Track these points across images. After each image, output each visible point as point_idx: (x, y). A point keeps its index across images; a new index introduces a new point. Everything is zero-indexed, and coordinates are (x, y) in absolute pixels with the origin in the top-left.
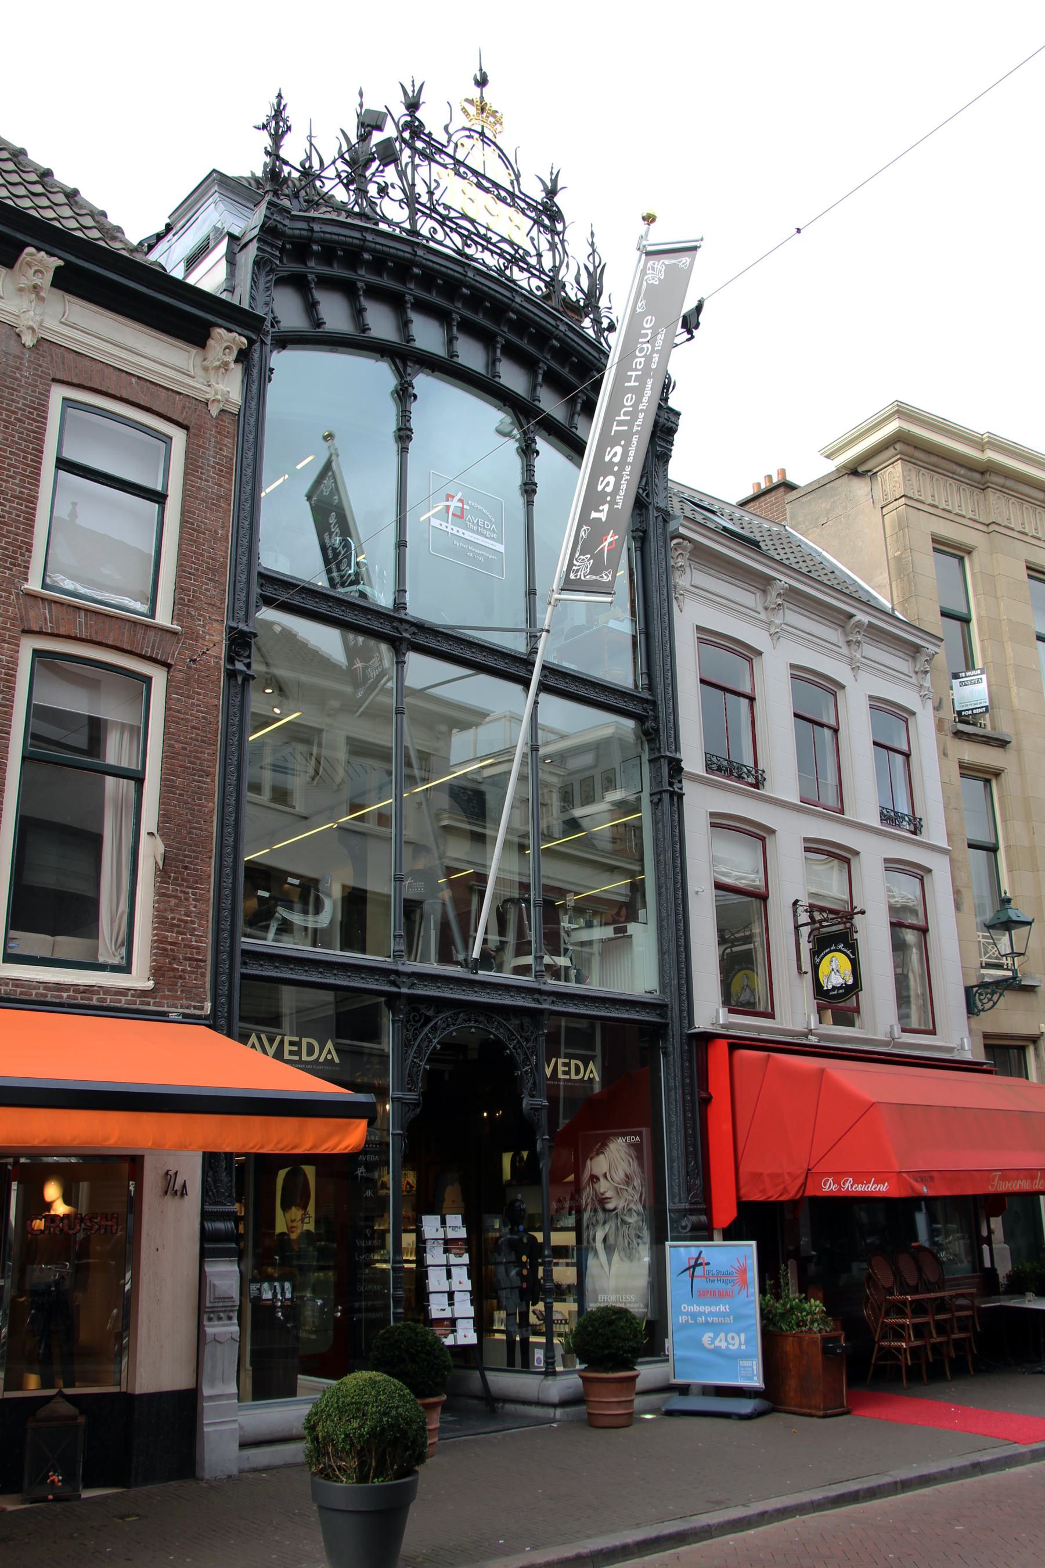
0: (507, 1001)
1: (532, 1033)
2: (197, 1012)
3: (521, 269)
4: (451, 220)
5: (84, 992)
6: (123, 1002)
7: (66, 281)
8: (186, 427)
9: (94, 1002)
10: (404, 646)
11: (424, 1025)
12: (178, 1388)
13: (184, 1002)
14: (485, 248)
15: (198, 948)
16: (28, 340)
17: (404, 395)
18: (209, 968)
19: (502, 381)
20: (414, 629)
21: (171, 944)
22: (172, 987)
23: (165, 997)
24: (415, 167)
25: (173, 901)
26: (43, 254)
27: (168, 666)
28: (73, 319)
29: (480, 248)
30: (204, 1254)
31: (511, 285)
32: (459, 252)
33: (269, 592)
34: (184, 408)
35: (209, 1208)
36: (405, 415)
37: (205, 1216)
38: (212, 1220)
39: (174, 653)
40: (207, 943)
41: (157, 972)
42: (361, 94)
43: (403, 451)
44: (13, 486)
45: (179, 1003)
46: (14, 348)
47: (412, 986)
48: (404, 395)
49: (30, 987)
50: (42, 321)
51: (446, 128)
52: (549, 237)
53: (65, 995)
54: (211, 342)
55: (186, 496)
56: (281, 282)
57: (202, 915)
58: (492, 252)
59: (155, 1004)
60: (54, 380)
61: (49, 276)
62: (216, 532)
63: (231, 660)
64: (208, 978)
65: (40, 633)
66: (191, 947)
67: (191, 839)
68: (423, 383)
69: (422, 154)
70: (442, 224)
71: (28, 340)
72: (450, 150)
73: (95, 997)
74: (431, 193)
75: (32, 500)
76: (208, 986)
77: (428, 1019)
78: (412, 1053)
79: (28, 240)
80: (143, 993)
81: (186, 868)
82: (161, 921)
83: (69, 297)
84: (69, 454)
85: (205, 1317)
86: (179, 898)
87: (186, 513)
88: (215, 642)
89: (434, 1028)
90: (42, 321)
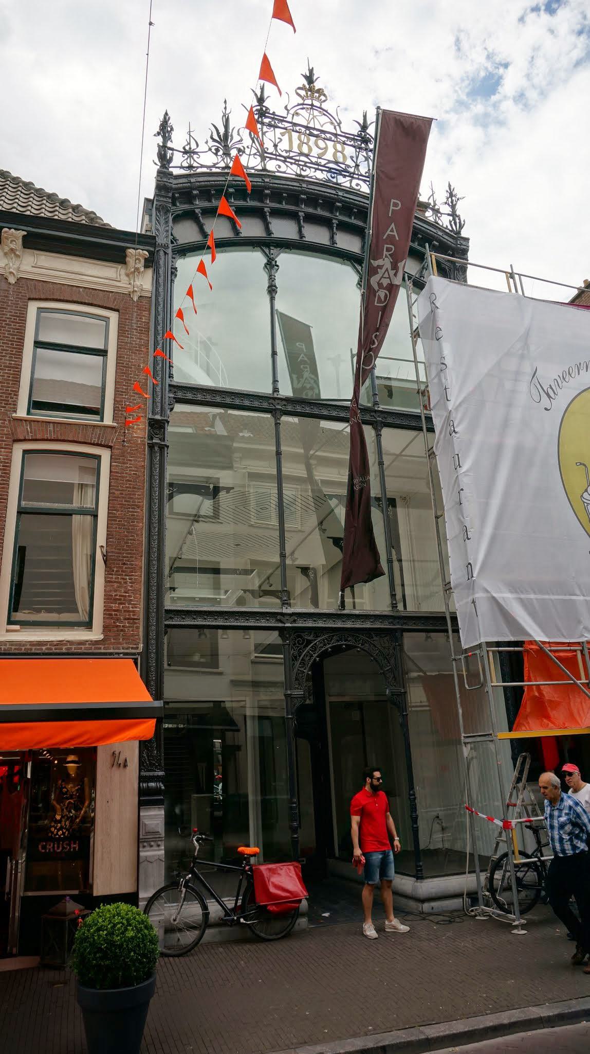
1: (62, 810)
2: (133, 651)
3: (345, 176)
4: (291, 158)
5: (57, 645)
6: (83, 649)
7: (30, 242)
8: (117, 310)
9: (64, 651)
10: (278, 412)
11: (306, 646)
12: (124, 892)
13: (125, 645)
15: (133, 611)
16: (12, 280)
17: (271, 265)
18: (141, 623)
19: (338, 246)
20: (284, 403)
21: (115, 611)
22: (116, 637)
23: (111, 644)
24: (263, 134)
25: (116, 585)
26: (13, 230)
27: (110, 447)
28: (40, 264)
29: (313, 170)
30: (142, 804)
31: (337, 187)
32: (297, 175)
33: (180, 395)
34: (115, 299)
35: (143, 774)
36: (271, 278)
37: (141, 779)
38: (144, 782)
39: (113, 439)
40: (140, 609)
41: (106, 628)
42: (225, 102)
43: (272, 299)
44: (6, 361)
45: (121, 646)
46: (4, 286)
47: (295, 621)
48: (271, 265)
49: (20, 645)
50: (19, 268)
51: (286, 108)
52: (364, 154)
53: (44, 648)
54: (128, 259)
55: (119, 348)
56: (177, 219)
57: (135, 591)
58: (322, 170)
59: (105, 648)
60: (30, 299)
61: (20, 241)
62: (139, 366)
63: (151, 438)
64: (141, 629)
65: (25, 440)
66: (129, 611)
67: (128, 546)
68: (284, 259)
69: (270, 125)
70: (284, 162)
71: (12, 280)
73: (64, 647)
74: (275, 146)
75: (17, 369)
76: (141, 634)
77: (309, 642)
78: (297, 664)
80: (97, 642)
81: (124, 564)
82: (108, 598)
83: (36, 252)
84: (43, 338)
85: (141, 845)
86: (120, 583)
87: (119, 357)
88: (140, 431)
89: (314, 649)
90: (19, 268)
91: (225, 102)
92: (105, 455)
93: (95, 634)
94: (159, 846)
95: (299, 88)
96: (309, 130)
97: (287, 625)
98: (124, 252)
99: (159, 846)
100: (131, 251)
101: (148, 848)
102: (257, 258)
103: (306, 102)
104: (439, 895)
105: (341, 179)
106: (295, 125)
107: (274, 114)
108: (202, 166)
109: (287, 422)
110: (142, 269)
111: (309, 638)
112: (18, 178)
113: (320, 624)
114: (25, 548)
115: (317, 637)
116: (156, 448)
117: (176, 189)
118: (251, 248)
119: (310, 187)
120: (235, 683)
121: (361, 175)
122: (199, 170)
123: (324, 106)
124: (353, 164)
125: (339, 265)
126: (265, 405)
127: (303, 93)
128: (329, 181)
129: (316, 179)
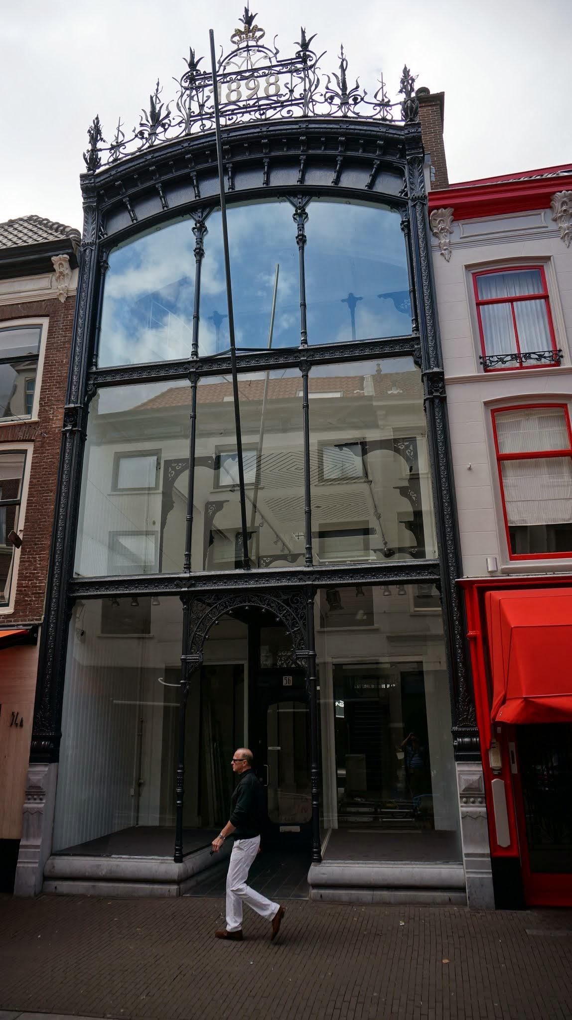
0: (273, 583)
14: (243, 113)
15: (40, 587)
17: (301, 215)
22: (24, 611)
23: (20, 616)
25: (27, 564)
27: (33, 441)
40: (45, 584)
42: (342, 47)
48: (301, 215)
63: (430, 393)
72: (274, 63)
79: (50, 254)
91: (342, 47)
92: (30, 448)
94: (41, 799)
95: (234, 36)
96: (253, 73)
99: (41, 799)
100: (54, 259)
101: (38, 801)
102: (286, 209)
103: (241, 46)
104: (396, 883)
105: (270, 113)
109: (250, 383)
116: (437, 401)
117: (99, 187)
118: (180, 218)
120: (393, 639)
123: (260, 43)
124: (287, 91)
125: (277, 205)
126: (181, 371)
128: (258, 120)
129: (244, 123)
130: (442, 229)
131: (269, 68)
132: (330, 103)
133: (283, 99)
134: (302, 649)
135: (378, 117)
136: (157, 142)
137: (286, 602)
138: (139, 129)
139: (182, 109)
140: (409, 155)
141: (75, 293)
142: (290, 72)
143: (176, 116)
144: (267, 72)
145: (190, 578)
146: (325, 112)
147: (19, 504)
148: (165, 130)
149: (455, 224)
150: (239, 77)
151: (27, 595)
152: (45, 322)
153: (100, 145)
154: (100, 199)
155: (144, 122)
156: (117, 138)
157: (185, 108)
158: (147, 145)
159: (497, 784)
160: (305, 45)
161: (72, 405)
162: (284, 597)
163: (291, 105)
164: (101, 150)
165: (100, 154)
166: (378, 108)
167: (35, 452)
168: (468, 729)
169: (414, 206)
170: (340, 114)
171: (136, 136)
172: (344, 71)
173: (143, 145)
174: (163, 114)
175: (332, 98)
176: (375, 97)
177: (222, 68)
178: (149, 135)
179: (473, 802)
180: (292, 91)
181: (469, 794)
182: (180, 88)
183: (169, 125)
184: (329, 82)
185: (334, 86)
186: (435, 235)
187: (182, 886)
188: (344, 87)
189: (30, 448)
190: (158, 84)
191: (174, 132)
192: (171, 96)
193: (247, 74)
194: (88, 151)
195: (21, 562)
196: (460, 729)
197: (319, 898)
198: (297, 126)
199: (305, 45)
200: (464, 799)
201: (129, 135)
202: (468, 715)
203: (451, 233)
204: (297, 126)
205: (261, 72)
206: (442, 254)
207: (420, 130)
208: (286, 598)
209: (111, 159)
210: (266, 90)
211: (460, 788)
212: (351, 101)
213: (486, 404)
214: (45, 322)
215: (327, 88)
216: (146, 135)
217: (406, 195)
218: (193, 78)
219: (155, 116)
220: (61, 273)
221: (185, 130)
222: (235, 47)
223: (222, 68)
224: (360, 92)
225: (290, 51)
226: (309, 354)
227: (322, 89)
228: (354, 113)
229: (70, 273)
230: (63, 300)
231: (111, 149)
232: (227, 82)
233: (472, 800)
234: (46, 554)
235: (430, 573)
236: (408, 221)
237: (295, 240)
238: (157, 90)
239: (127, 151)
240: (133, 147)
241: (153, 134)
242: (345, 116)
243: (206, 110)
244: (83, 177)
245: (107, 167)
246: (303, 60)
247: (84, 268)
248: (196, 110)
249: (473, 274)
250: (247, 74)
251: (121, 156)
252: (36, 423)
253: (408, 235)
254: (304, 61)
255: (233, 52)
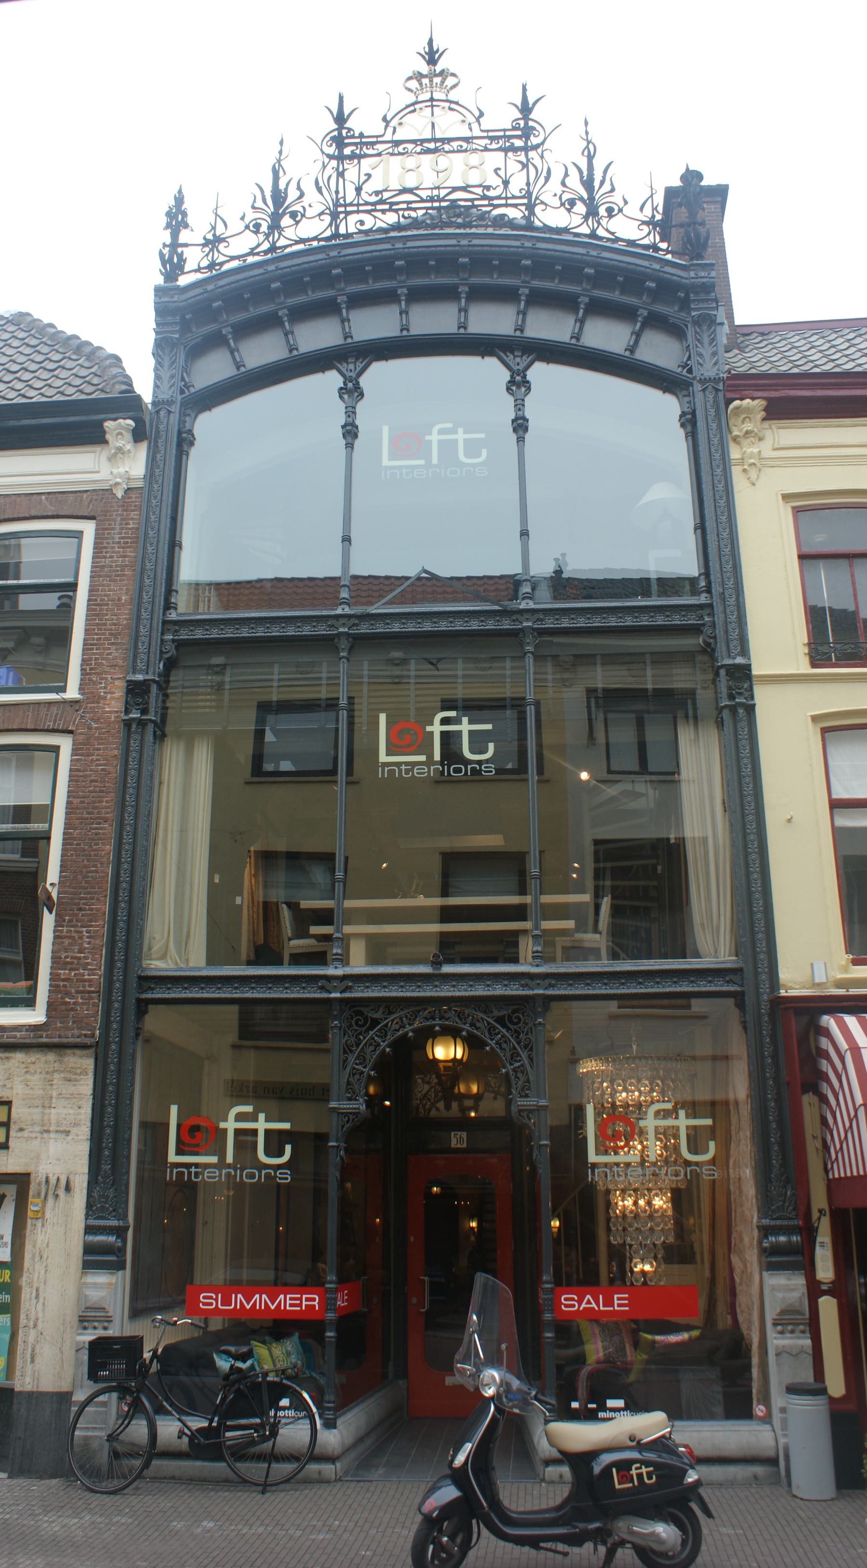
11: (371, 1028)
13: (76, 1032)
15: (90, 980)
21: (63, 980)
23: (56, 1029)
25: (67, 941)
27: (71, 732)
36: (351, 412)
41: (51, 1007)
42: (586, 123)
48: (518, 384)
51: (384, 119)
54: (108, 437)
61: (129, 436)
62: (120, 599)
63: (127, 711)
67: (87, 882)
68: (541, 373)
72: (477, 132)
77: (375, 1022)
81: (80, 909)
91: (586, 123)
92: (65, 744)
93: (36, 1016)
97: (333, 995)
98: (102, 426)
100: (109, 425)
106: (397, 143)
107: (361, 135)
108: (233, 258)
110: (129, 447)
111: (376, 1016)
112: (153, 354)
113: (394, 992)
114: (443, 701)
115: (390, 1013)
119: (410, 244)
121: (514, 197)
122: (226, 267)
123: (452, 96)
124: (499, 182)
127: (413, 84)
130: (747, 432)
131: (466, 140)
132: (569, 211)
133: (492, 193)
134: (527, 1096)
135: (646, 242)
136: (282, 242)
137: (500, 1020)
138: (251, 216)
139: (324, 190)
140: (695, 310)
141: (140, 484)
142: (505, 150)
143: (314, 202)
144: (465, 145)
145: (345, 977)
146: (562, 225)
147: (48, 838)
148: (297, 223)
149: (767, 424)
150: (418, 149)
151: (68, 994)
152: (88, 529)
153: (184, 236)
154: (185, 327)
155: (259, 204)
156: (214, 228)
157: (329, 190)
158: (266, 246)
159: (828, 1307)
160: (526, 109)
161: (140, 677)
162: (496, 1013)
163: (506, 205)
164: (186, 245)
165: (187, 252)
166: (646, 229)
167: (75, 751)
168: (785, 1223)
169: (704, 390)
170: (585, 230)
171: (247, 227)
172: (590, 158)
173: (259, 245)
174: (293, 194)
175: (572, 202)
176: (641, 209)
177: (390, 130)
178: (269, 228)
179: (792, 1332)
180: (506, 183)
181: (786, 1320)
182: (319, 155)
183: (303, 216)
184: (566, 175)
185: (574, 181)
186: (735, 439)
187: (338, 1465)
188: (588, 184)
189: (65, 744)
190: (281, 143)
191: (314, 227)
192: (306, 165)
193: (432, 146)
194: (165, 245)
195: (55, 937)
196: (773, 1223)
197: (557, 1479)
198: (518, 243)
199: (526, 109)
200: (779, 1328)
201: (236, 226)
202: (784, 1201)
203: (760, 439)
204: (518, 243)
205: (455, 144)
206: (744, 471)
207: (713, 274)
208: (502, 1013)
209: (205, 263)
210: (464, 175)
211: (770, 1315)
212: (602, 211)
213: (815, 719)
214: (88, 529)
215: (563, 184)
216: (264, 228)
217: (690, 371)
218: (345, 143)
219: (279, 197)
220: (120, 450)
221: (330, 225)
222: (411, 98)
223: (390, 130)
224: (617, 198)
225: (502, 117)
226: (537, 616)
227: (554, 185)
228: (607, 230)
229: (133, 451)
230: (119, 494)
231: (204, 245)
232: (400, 154)
233: (790, 1328)
234: (101, 927)
235: (728, 982)
236: (693, 413)
237: (340, 432)
238: (280, 153)
239: (233, 251)
240: (241, 245)
241: (275, 226)
242: (593, 235)
243: (365, 196)
244: (158, 290)
245: (200, 276)
246: (522, 135)
247: (156, 442)
248: (351, 196)
249: (793, 508)
250: (432, 146)
251: (222, 259)
252: (75, 702)
253: (692, 435)
254: (527, 133)
255: (407, 107)
